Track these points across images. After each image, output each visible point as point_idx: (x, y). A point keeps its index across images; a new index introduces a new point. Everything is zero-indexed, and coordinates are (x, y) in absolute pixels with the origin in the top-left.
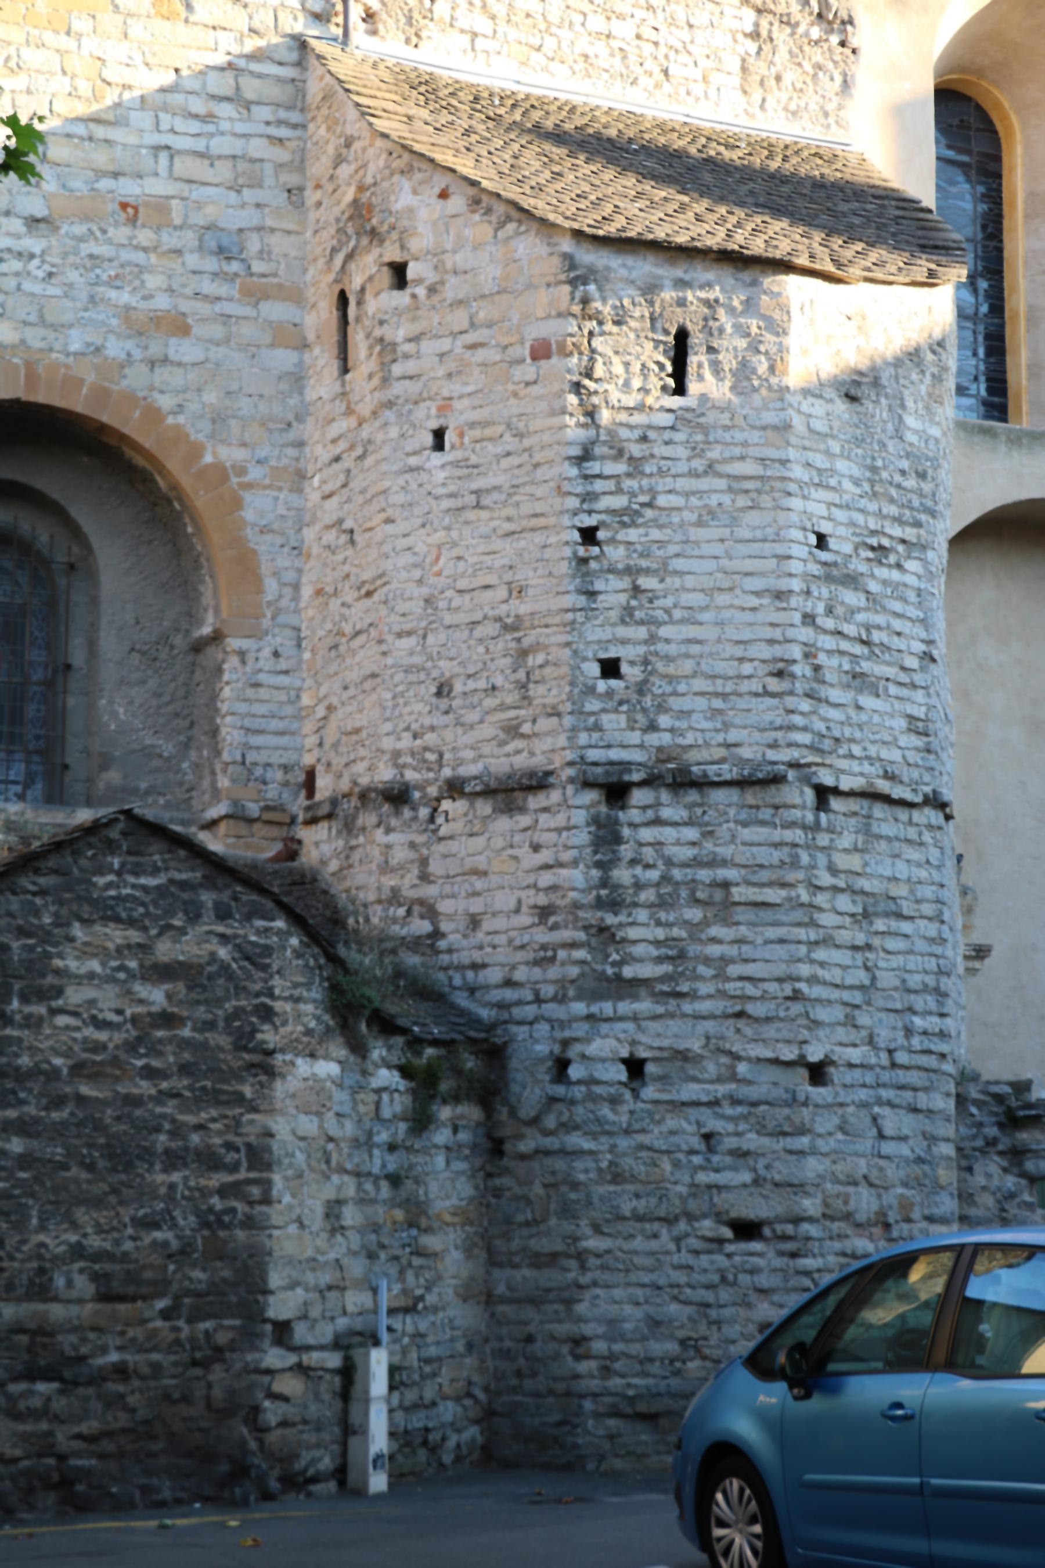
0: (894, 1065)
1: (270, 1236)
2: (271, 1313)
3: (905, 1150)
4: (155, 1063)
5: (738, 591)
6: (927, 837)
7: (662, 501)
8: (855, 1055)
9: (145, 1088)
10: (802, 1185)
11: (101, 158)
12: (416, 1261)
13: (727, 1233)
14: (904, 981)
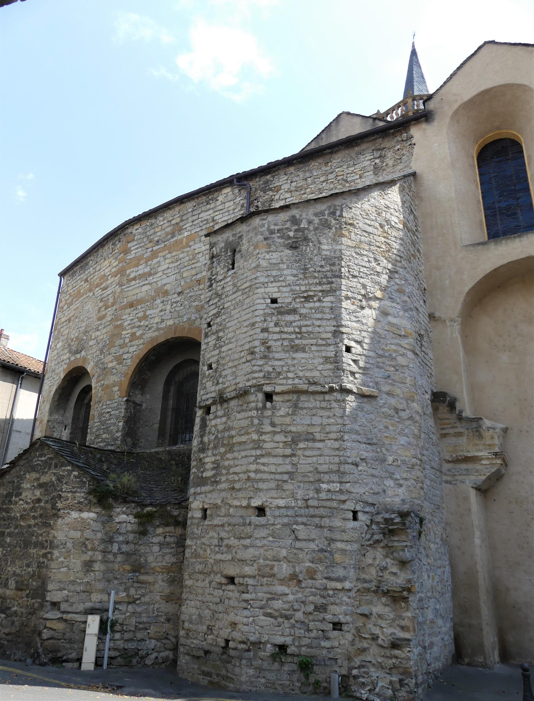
0: (308, 507)
1: (51, 572)
2: (48, 599)
3: (313, 546)
4: (35, 514)
5: (242, 328)
6: (334, 405)
7: (226, 306)
8: (281, 503)
9: (32, 522)
10: (246, 561)
11: (194, 272)
12: (136, 585)
13: (224, 581)
14: (316, 468)
